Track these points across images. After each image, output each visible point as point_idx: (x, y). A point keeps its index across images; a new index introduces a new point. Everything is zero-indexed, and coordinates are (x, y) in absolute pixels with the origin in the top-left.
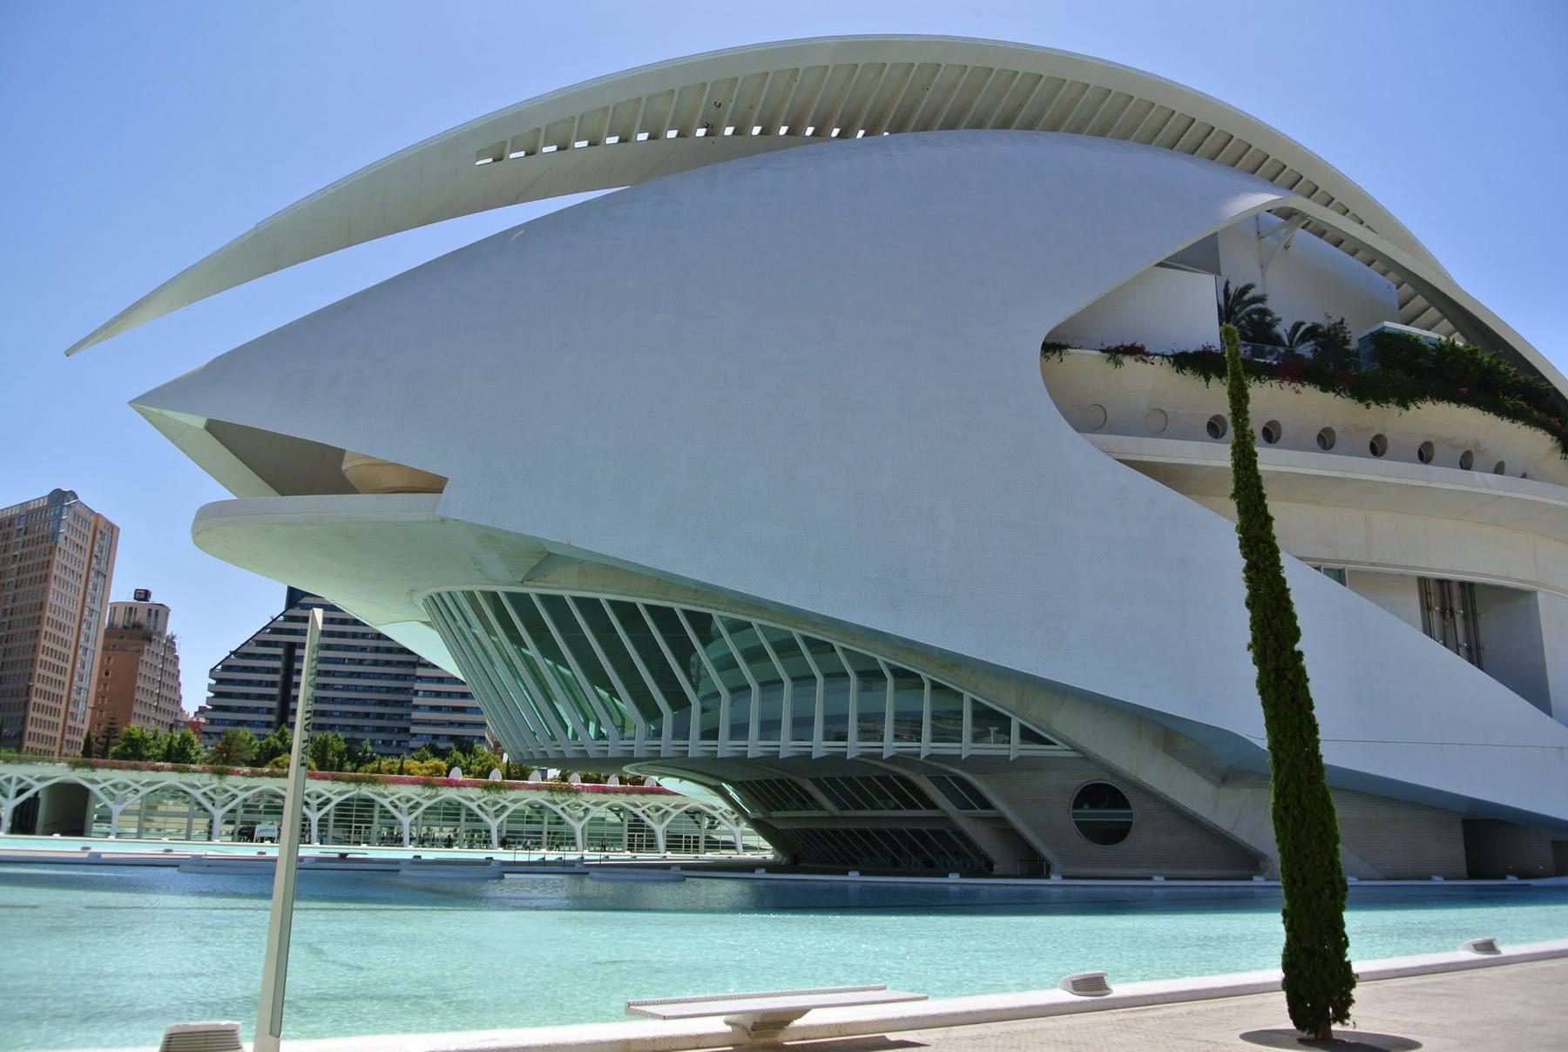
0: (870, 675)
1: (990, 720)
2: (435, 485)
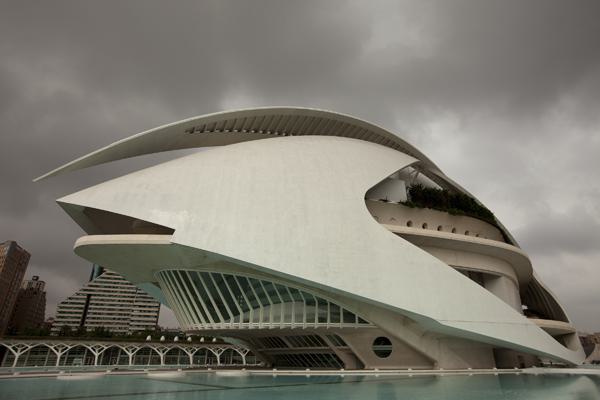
1: (349, 317)
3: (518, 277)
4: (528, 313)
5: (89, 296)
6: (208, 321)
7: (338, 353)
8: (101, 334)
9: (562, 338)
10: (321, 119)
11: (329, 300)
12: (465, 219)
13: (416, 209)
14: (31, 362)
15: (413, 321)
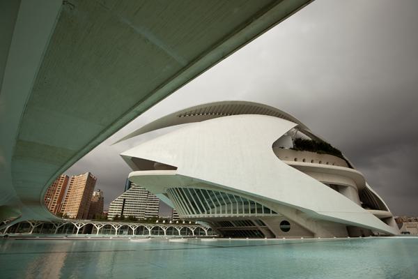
0: (246, 203)
1: (267, 210)
2: (175, 168)
3: (357, 187)
4: (364, 206)
5: (125, 199)
6: (193, 213)
7: (261, 230)
8: (132, 219)
9: (385, 220)
10: (262, 108)
11: (256, 201)
12: (326, 155)
13: (299, 151)
14: (105, 232)
15: (302, 212)
